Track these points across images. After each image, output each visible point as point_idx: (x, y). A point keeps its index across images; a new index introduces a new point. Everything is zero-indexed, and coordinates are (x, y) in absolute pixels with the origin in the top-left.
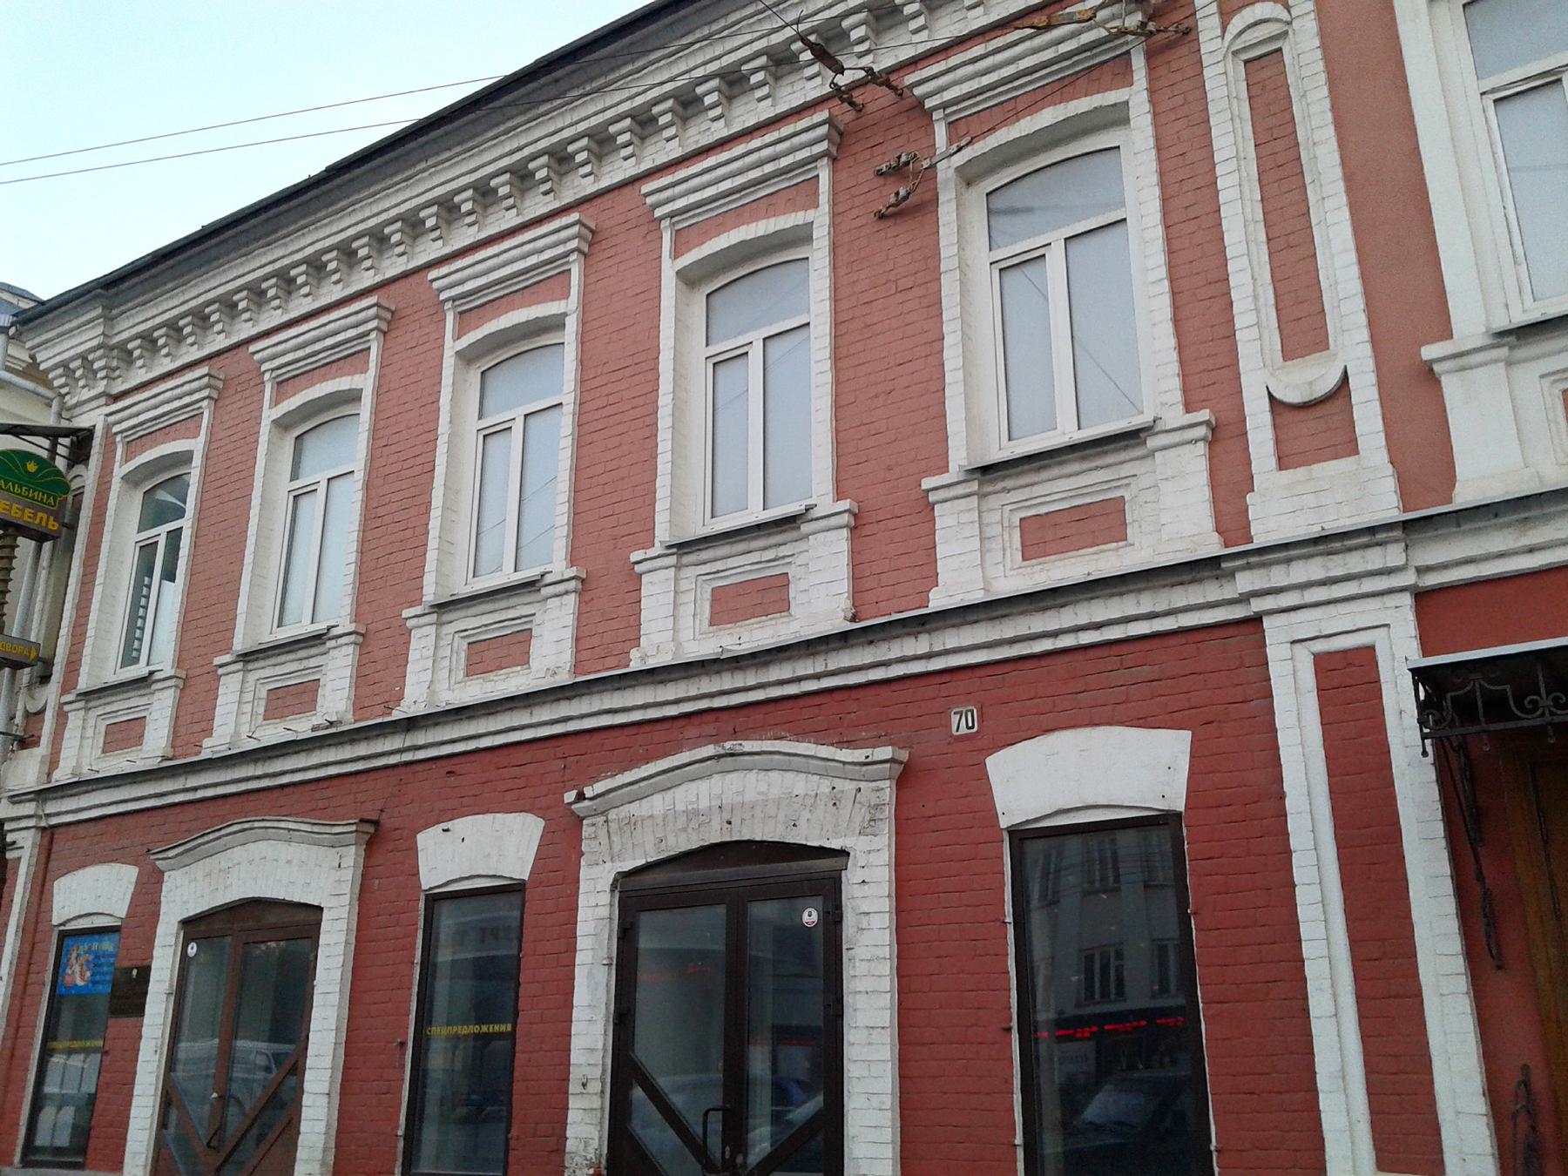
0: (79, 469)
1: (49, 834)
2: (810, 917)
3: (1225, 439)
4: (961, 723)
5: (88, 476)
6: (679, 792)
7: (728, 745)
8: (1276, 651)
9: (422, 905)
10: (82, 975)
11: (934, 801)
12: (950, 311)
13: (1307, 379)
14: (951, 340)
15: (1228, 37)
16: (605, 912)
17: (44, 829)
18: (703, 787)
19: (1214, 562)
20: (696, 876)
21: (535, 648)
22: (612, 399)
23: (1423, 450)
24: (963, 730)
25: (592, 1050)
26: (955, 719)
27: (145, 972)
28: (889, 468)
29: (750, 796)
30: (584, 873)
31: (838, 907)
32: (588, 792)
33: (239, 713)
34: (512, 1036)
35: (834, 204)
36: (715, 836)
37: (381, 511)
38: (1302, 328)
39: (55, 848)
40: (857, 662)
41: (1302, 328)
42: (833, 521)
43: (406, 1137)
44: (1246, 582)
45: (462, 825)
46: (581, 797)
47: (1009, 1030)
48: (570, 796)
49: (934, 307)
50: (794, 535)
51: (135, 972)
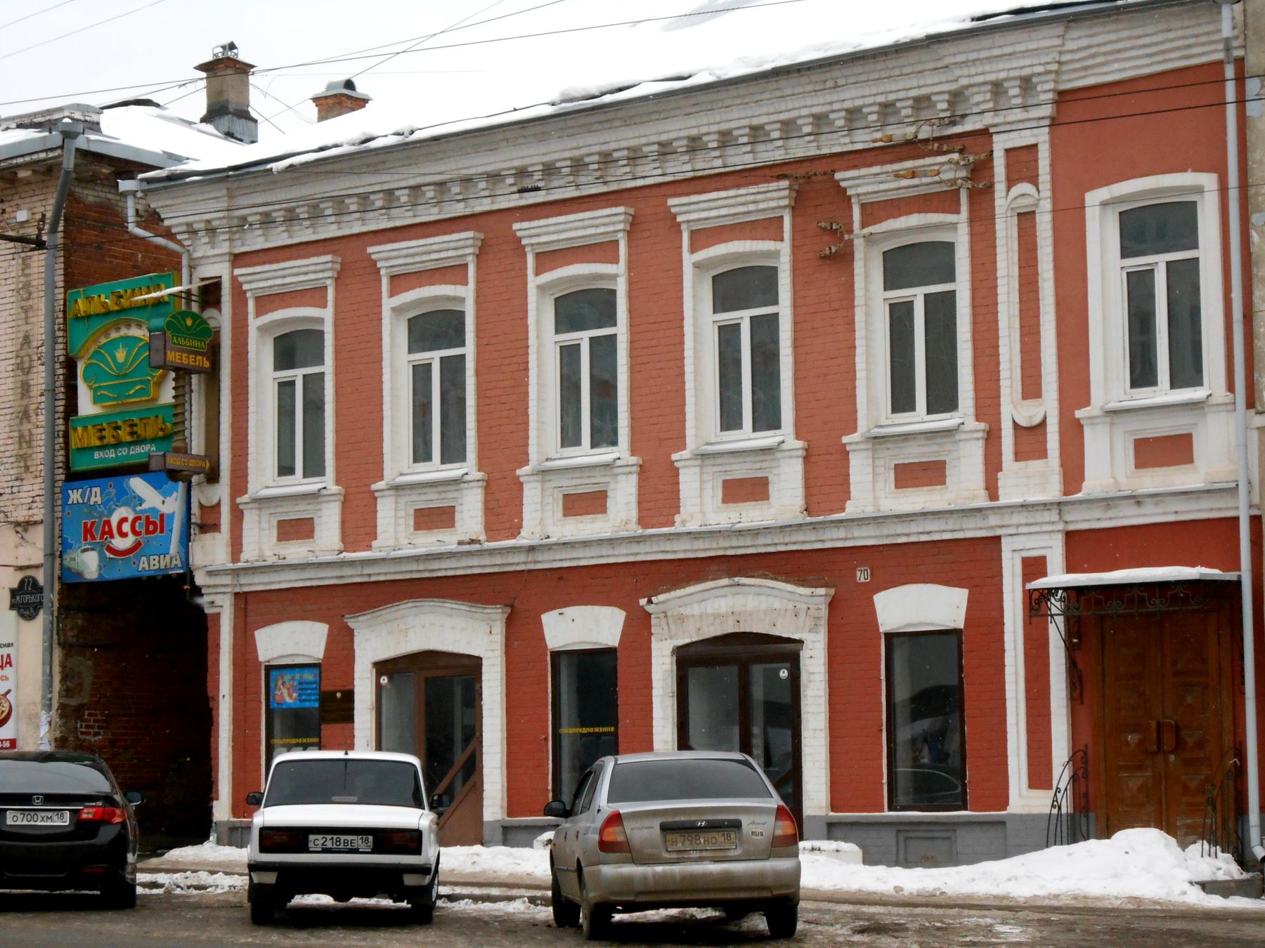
0: (210, 313)
1: (243, 600)
2: (784, 674)
3: (992, 439)
4: (862, 576)
5: (223, 319)
6: (709, 603)
7: (736, 579)
8: (1006, 555)
9: (549, 658)
10: (290, 696)
11: (849, 622)
12: (860, 333)
13: (1029, 414)
14: (860, 351)
15: (1010, 198)
16: (668, 667)
17: (236, 594)
18: (723, 601)
19: (979, 510)
20: (721, 649)
21: (610, 503)
22: (653, 343)
23: (1073, 473)
24: (862, 580)
25: (666, 742)
26: (858, 573)
27: (349, 696)
28: (825, 423)
29: (749, 608)
30: (654, 645)
31: (798, 669)
32: (654, 599)
33: (396, 525)
34: (616, 734)
35: (793, 239)
36: (730, 628)
37: (490, 393)
38: (1031, 389)
39: (249, 607)
40: (807, 539)
41: (1031, 389)
42: (794, 453)
43: (553, 790)
44: (993, 520)
45: (572, 611)
46: (650, 602)
47: (881, 731)
48: (643, 602)
49: (851, 323)
50: (771, 457)
51: (339, 695)
